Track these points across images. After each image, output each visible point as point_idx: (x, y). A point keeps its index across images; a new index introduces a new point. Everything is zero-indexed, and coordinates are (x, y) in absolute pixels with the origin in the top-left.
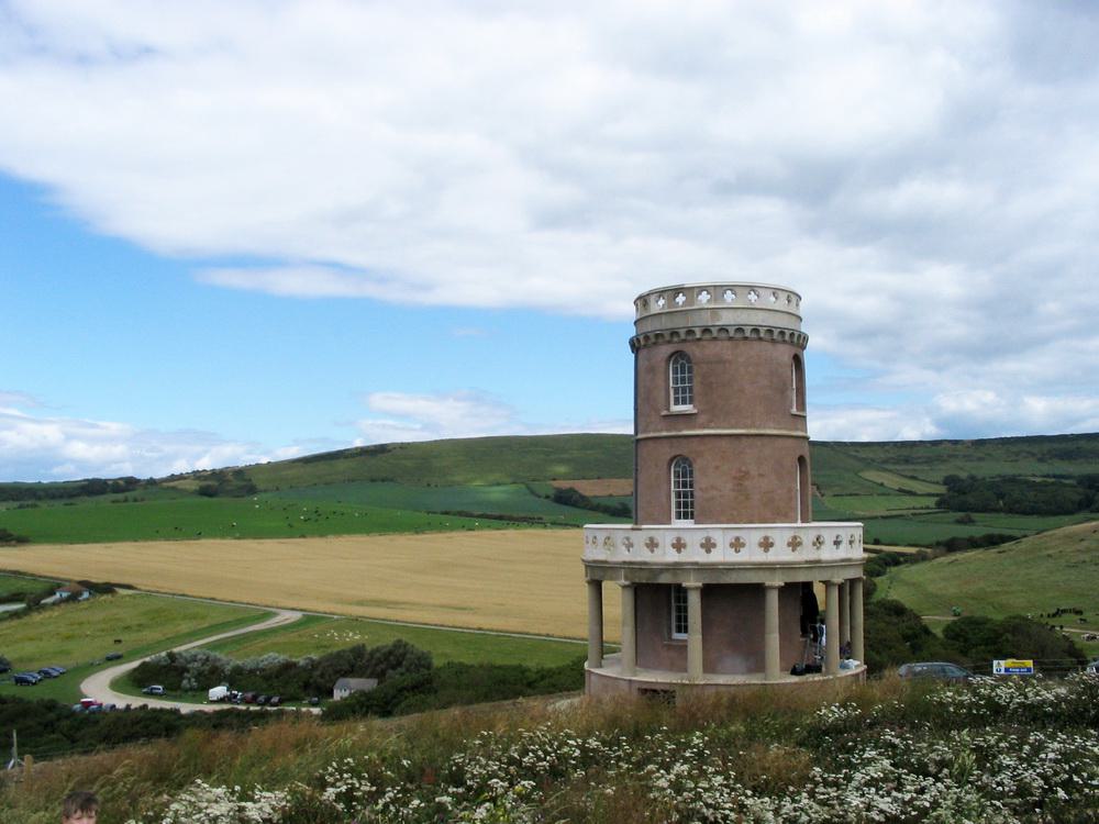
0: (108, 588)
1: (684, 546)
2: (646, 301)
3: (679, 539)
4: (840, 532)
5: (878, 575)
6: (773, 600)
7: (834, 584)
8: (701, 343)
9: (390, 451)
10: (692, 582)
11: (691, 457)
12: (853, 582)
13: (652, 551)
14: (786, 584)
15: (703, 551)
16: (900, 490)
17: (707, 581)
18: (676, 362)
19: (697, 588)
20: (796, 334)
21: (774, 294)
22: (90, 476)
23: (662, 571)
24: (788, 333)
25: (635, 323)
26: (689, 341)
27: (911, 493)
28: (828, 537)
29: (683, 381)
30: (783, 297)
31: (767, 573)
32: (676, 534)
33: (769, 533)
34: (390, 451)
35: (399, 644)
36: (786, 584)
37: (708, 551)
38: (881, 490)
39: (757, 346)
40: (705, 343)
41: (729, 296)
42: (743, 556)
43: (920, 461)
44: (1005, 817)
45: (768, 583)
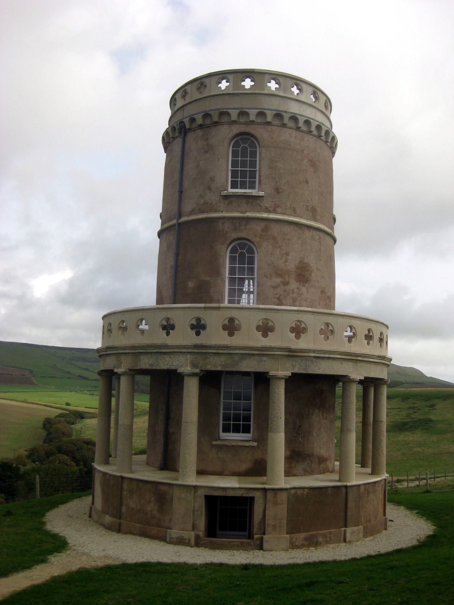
0: (90, 394)
1: (204, 327)
5: (73, 424)
6: (231, 390)
7: (352, 381)
8: (270, 128)
13: (168, 334)
14: (292, 374)
15: (194, 332)
17: (296, 370)
19: (194, 375)
20: (324, 129)
22: (336, 220)
23: (244, 356)
26: (258, 124)
27: (87, 379)
29: (244, 164)
31: (350, 364)
33: (169, 314)
36: (292, 374)
37: (231, 334)
39: (307, 138)
40: (274, 128)
41: (273, 85)
44: (81, 550)
45: (272, 373)
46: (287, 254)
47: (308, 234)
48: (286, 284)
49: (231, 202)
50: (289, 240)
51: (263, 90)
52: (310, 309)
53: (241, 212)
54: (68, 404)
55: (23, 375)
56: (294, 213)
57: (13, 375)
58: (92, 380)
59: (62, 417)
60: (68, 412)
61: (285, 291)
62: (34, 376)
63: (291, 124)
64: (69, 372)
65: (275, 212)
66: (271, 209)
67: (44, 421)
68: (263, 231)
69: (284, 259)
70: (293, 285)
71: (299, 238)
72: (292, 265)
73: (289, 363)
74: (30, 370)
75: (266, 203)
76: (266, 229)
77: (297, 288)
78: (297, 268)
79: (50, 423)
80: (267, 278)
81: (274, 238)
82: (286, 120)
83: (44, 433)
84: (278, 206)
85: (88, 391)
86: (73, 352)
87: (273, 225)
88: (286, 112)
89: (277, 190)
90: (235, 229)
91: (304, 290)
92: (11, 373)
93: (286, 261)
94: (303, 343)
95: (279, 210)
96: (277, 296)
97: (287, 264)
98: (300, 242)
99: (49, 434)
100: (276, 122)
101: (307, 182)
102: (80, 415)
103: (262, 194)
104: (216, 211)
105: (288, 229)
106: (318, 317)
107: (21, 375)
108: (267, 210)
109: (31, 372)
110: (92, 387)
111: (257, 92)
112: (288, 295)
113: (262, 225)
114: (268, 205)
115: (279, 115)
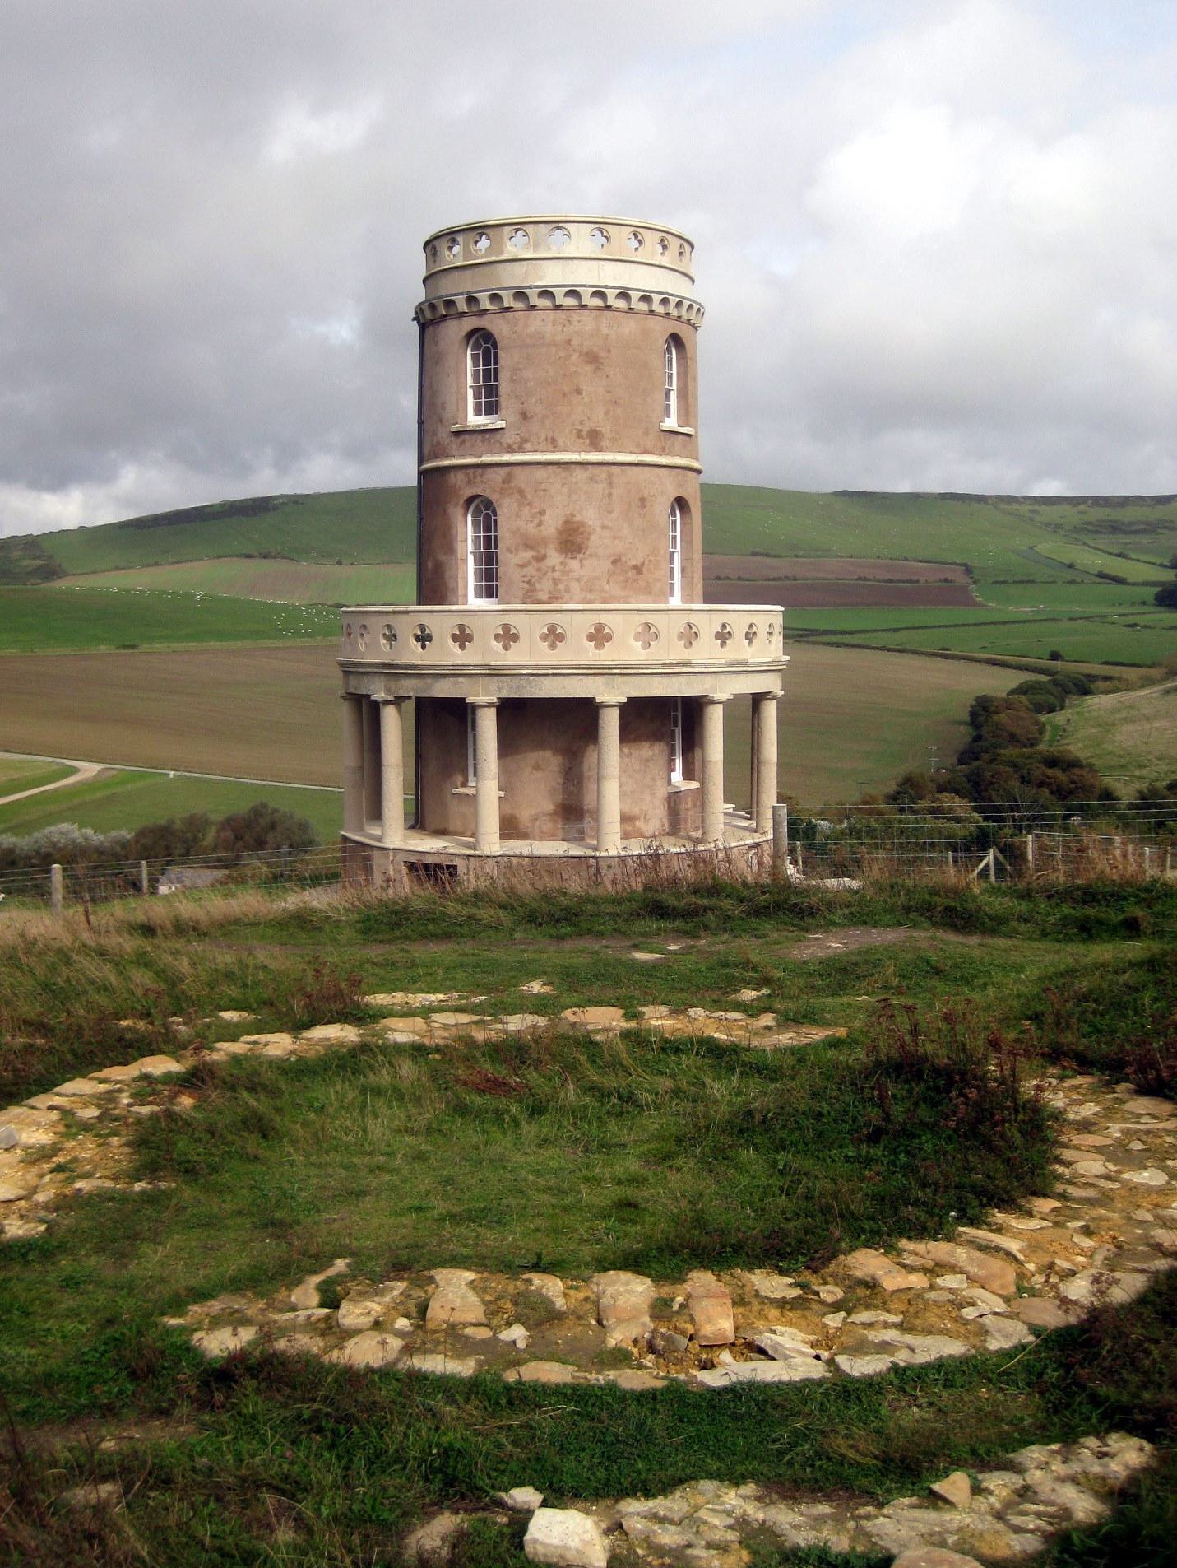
2: (434, 247)
3: (461, 627)
4: (754, 619)
5: (1051, 710)
9: (275, 508)
10: (484, 696)
11: (493, 497)
12: (757, 700)
16: (1101, 575)
17: (505, 694)
18: (476, 348)
19: (490, 705)
21: (635, 235)
24: (686, 303)
25: (425, 281)
27: (1120, 581)
28: (739, 629)
30: (651, 239)
32: (457, 620)
34: (275, 508)
35: (258, 812)
38: (1068, 575)
42: (562, 656)
43: (1134, 528)
46: (542, 513)
47: (580, 474)
48: (541, 558)
49: (463, 442)
50: (545, 490)
51: (501, 253)
52: (523, 607)
53: (476, 457)
54: (1055, 656)
55: (946, 580)
56: (554, 445)
57: (917, 581)
58: (1134, 584)
59: (1025, 693)
60: (1044, 678)
61: (539, 570)
62: (975, 583)
63: (545, 303)
64: (1071, 566)
65: (521, 450)
66: (515, 447)
67: (972, 706)
68: (504, 482)
69: (536, 521)
70: (554, 558)
71: (563, 485)
72: (551, 526)
73: (493, 683)
74: (965, 565)
75: (509, 438)
76: (508, 479)
77: (561, 563)
78: (560, 533)
79: (985, 709)
80: (511, 552)
81: (521, 492)
82: (534, 300)
83: (964, 734)
84: (526, 441)
85: (1121, 615)
86: (1082, 507)
87: (517, 470)
88: (529, 287)
89: (524, 416)
90: (469, 482)
91: (574, 564)
92: (915, 578)
93: (540, 524)
94: (516, 656)
95: (528, 446)
96: (527, 579)
97: (542, 528)
98: (565, 490)
99: (978, 739)
100: (519, 305)
101: (579, 392)
102: (1076, 685)
103: (501, 424)
104: (448, 456)
105: (540, 473)
106: (536, 616)
107: (940, 581)
108: (510, 450)
109: (968, 570)
110: (1133, 604)
111: (494, 258)
112: (544, 575)
113: (503, 471)
114: (510, 441)
115: (520, 295)
